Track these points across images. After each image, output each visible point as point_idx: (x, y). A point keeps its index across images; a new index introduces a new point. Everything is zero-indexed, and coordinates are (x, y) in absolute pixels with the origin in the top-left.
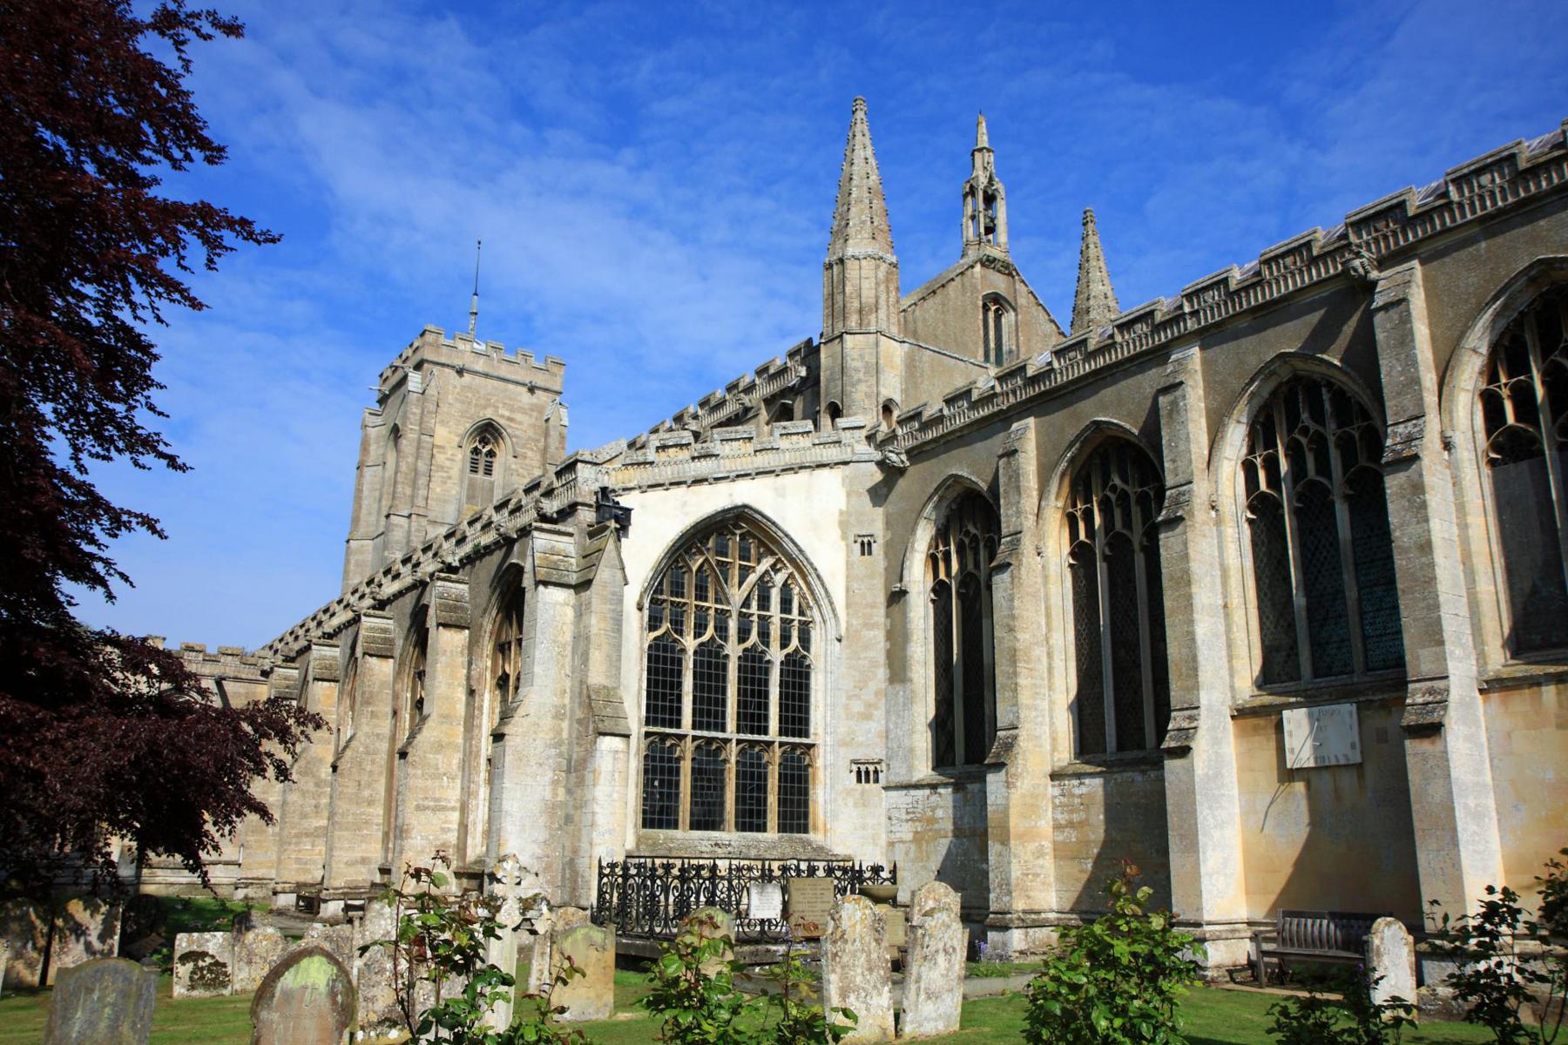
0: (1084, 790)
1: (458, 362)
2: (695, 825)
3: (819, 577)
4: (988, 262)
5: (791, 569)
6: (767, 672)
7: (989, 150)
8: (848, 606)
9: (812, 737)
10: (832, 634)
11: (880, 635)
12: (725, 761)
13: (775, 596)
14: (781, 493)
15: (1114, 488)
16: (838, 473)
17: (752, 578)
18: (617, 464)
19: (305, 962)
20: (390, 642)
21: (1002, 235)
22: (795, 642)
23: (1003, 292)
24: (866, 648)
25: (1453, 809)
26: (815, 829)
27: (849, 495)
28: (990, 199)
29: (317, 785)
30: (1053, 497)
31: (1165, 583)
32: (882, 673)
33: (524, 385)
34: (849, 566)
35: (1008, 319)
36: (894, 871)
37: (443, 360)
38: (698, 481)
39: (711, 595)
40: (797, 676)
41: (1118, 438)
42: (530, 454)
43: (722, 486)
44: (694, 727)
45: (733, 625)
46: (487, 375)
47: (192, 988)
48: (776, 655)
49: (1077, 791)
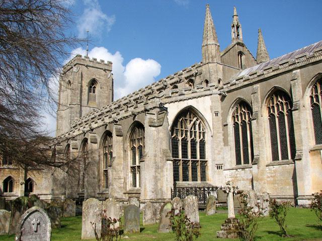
0: (274, 169)
1: (86, 64)
2: (183, 180)
4: (238, 44)
5: (200, 120)
6: (177, 143)
7: (237, 16)
10: (211, 135)
11: (221, 135)
12: (189, 165)
13: (197, 126)
14: (198, 102)
15: (279, 101)
16: (209, 96)
17: (192, 123)
18: (163, 97)
19: (167, 204)
20: (96, 139)
21: (241, 37)
22: (202, 137)
23: (242, 51)
24: (218, 138)
26: (208, 180)
27: (212, 102)
28: (238, 27)
30: (264, 103)
31: (294, 123)
32: (222, 144)
33: (102, 69)
35: (243, 57)
37: (82, 63)
38: (180, 101)
39: (184, 127)
40: (203, 143)
41: (280, 90)
42: (105, 87)
43: (185, 101)
44: (183, 157)
45: (189, 133)
46: (93, 67)
48: (198, 140)
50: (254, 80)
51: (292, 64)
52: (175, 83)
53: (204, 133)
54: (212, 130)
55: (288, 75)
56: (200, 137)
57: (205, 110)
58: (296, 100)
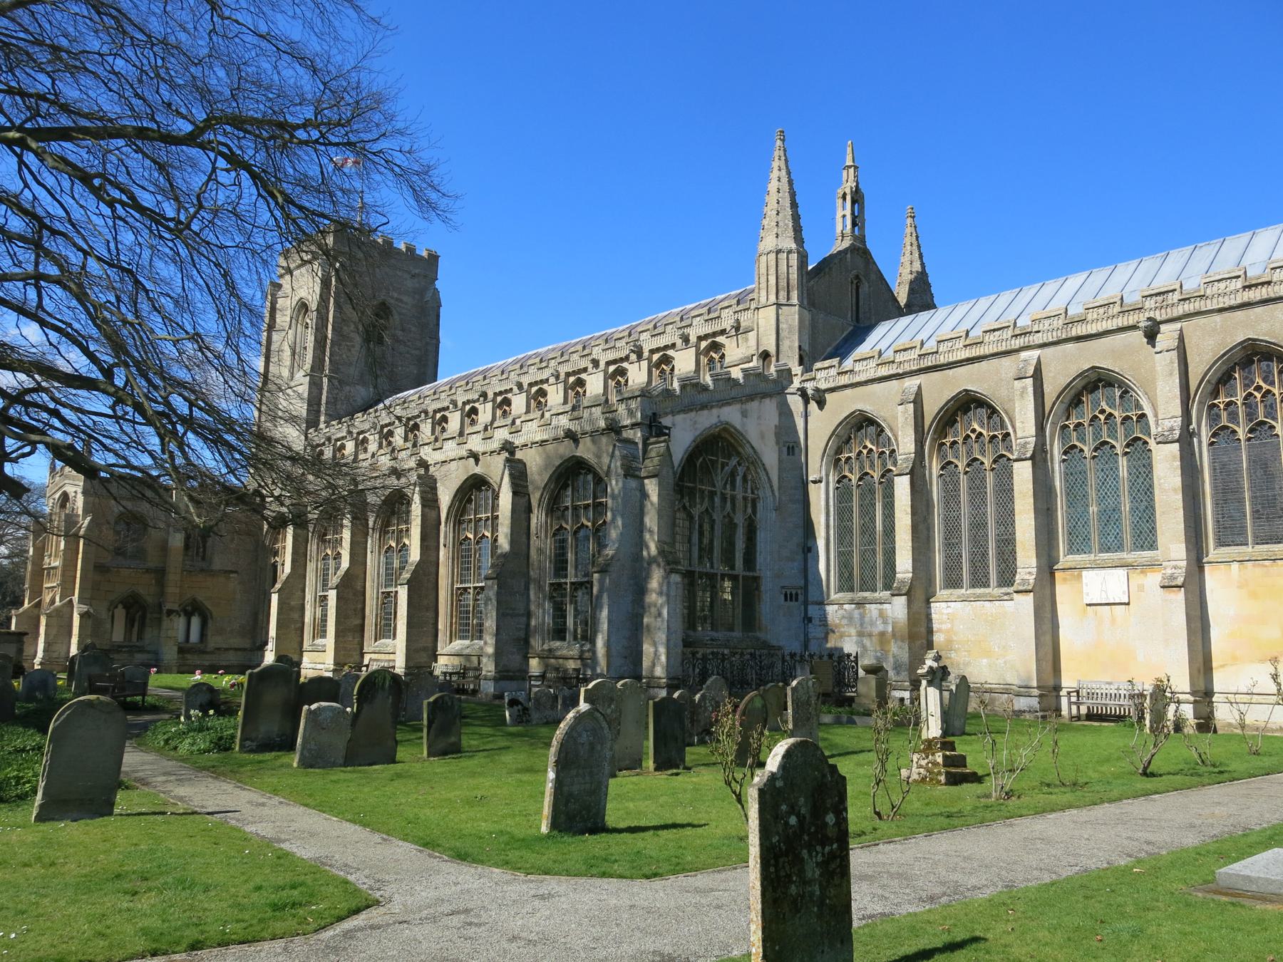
0: (950, 610)
3: (765, 469)
8: (779, 488)
9: (946, 592)
25: (436, 489)
26: (760, 629)
29: (354, 594)
34: (780, 461)
36: (856, 657)
42: (413, 329)
47: (894, 657)
48: (739, 519)
49: (945, 611)
50: (907, 368)
51: (1021, 335)
52: (666, 347)
53: (754, 502)
54: (777, 494)
55: (1006, 361)
56: (723, 508)
57: (762, 436)
58: (1024, 434)
